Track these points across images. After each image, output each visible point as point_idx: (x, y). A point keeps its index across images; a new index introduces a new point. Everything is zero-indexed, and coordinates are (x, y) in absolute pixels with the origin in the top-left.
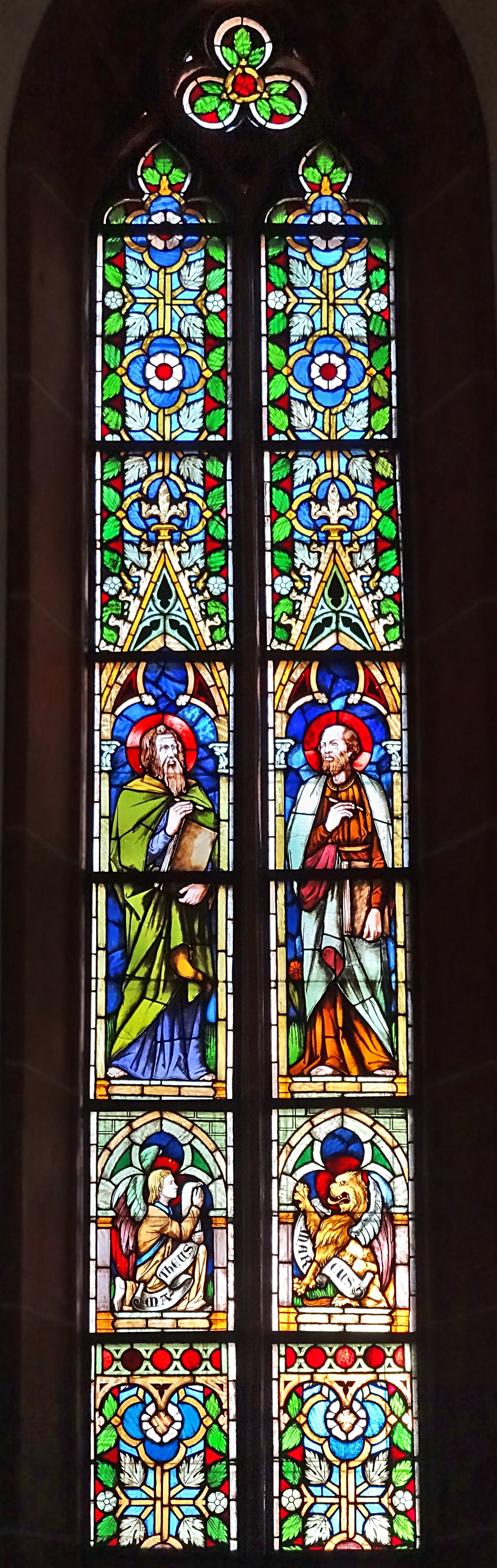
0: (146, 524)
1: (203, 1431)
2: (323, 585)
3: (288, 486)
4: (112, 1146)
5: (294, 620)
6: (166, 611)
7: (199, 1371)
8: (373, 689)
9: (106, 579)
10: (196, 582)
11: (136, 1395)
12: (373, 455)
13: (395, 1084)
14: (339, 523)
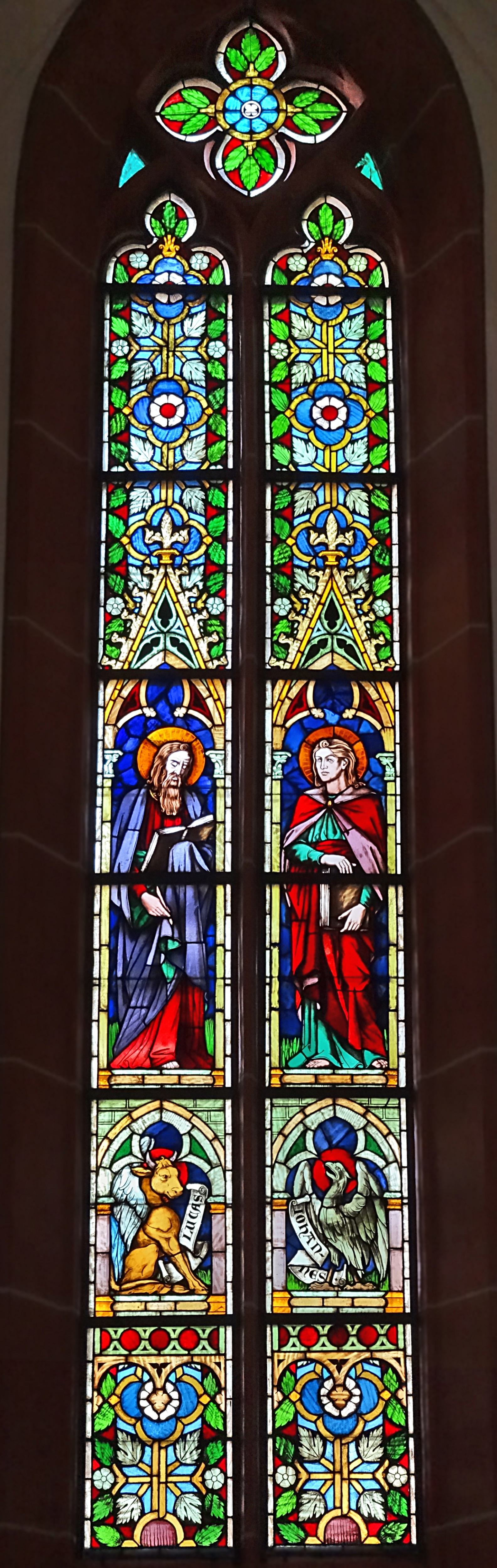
0: (149, 549)
1: (200, 1408)
2: (153, 606)
3: (289, 515)
4: (286, 1132)
5: (291, 639)
6: (165, 630)
7: (197, 1351)
8: (367, 705)
9: (275, 600)
10: (361, 604)
11: (135, 1374)
12: (371, 487)
13: (386, 1076)
14: (337, 550)
